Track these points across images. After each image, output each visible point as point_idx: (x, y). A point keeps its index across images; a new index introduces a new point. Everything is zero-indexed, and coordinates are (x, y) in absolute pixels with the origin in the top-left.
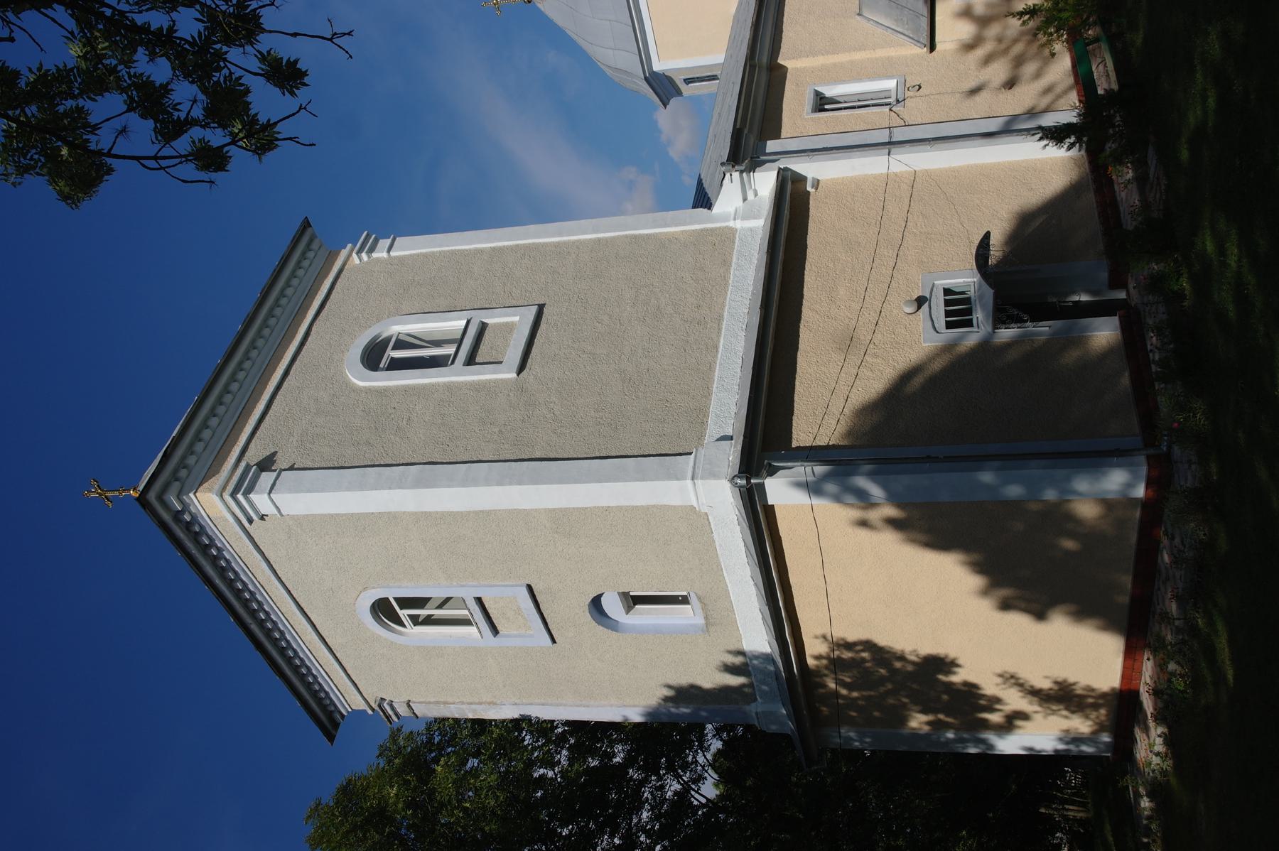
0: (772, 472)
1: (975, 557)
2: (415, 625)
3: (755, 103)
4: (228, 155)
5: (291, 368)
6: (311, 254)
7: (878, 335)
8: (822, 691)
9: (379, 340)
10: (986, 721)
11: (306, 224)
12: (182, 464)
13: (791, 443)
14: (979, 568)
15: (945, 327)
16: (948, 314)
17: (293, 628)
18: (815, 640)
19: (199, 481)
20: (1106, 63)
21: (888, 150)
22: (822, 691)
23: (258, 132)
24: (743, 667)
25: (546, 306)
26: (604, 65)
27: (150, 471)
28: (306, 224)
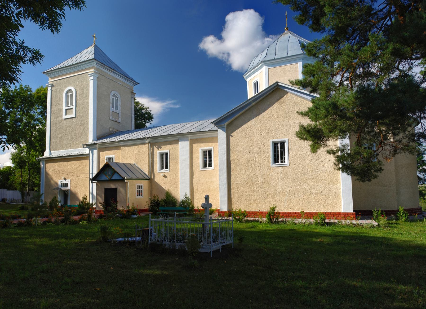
0: (57, 184)
1: (233, 71)
2: (44, 156)
3: (110, 145)
4: (37, 50)
5: (154, 163)
6: (90, 64)
7: (61, 174)
8: (306, 41)
9: (97, 72)
10: (11, 83)
11: (138, 84)
12: (51, 73)
13: (232, 133)
14: (232, 12)
15: (106, 187)
16: (63, 184)
17: (285, 84)
18: (288, 81)
19: (221, 127)
20: (135, 107)
21: (48, 165)
22: (306, 41)
23: (358, 35)
24: (306, 70)
25: (218, 42)
26: (248, 228)
27: (207, 135)
28: (138, 84)
